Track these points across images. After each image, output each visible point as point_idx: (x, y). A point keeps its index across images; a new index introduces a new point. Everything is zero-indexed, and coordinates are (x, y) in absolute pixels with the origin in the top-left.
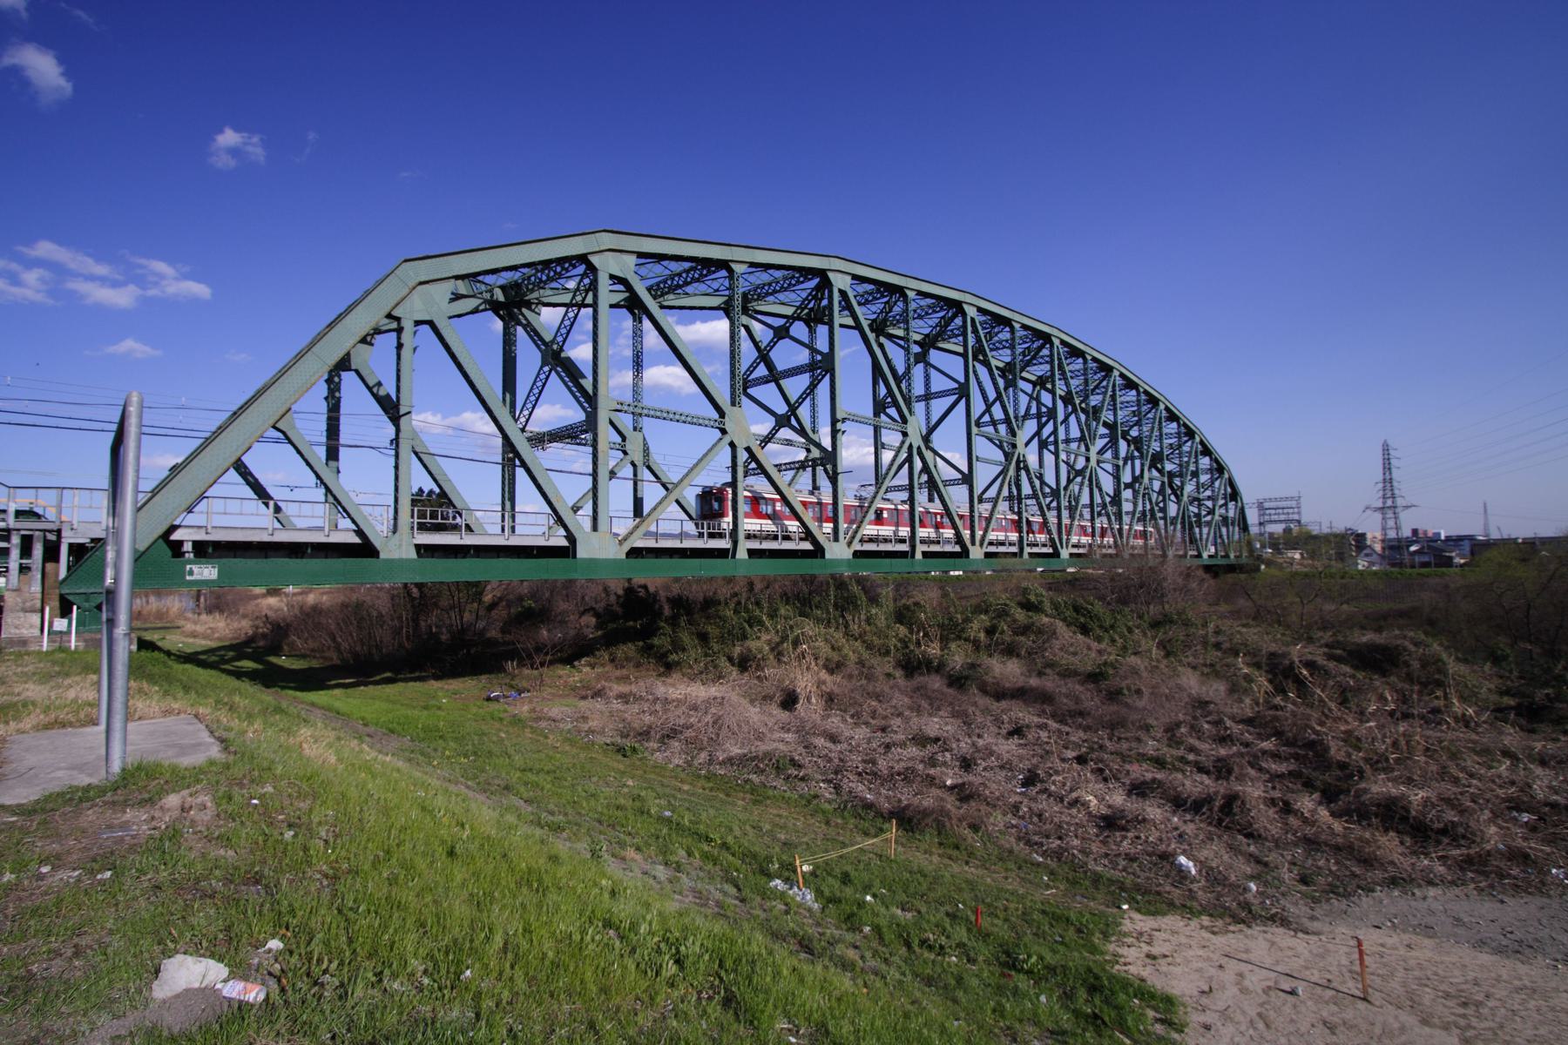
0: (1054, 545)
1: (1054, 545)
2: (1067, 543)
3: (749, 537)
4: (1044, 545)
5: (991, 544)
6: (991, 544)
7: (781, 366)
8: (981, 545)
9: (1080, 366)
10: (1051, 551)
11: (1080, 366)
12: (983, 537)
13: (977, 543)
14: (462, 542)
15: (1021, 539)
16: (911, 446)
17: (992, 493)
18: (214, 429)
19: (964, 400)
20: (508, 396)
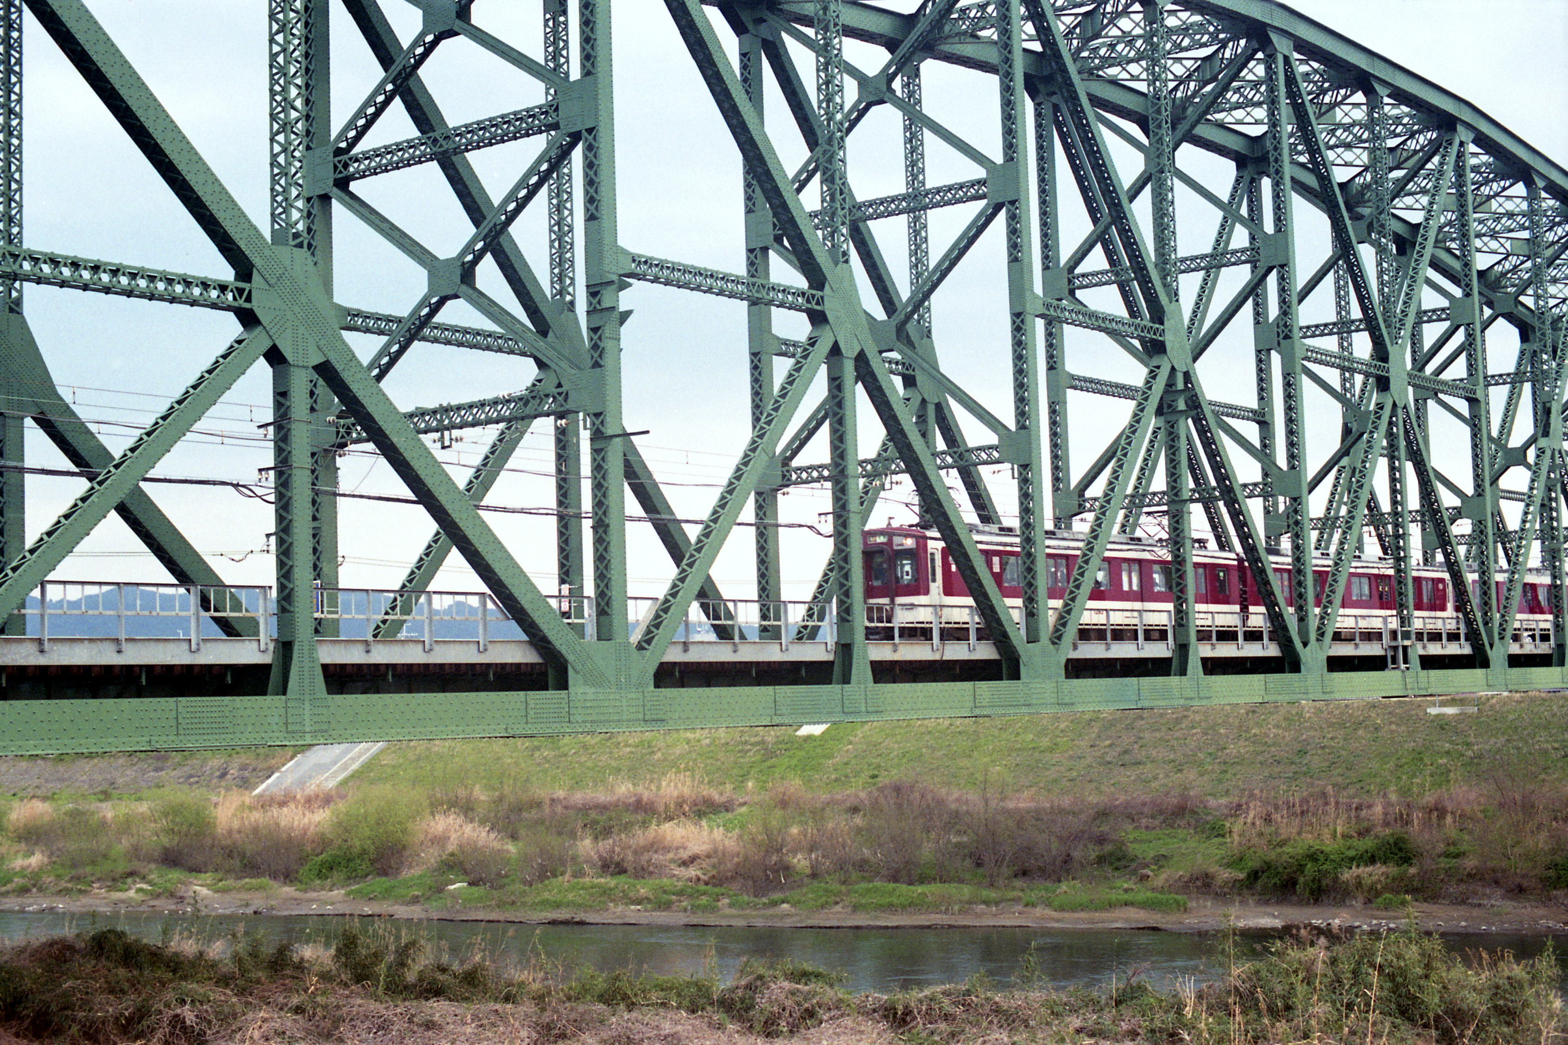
0: (1473, 636)
1: (1286, 643)
2: (1321, 634)
3: (1204, 635)
4: (1453, 637)
5: (1085, 634)
6: (1337, 637)
7: (898, 186)
8: (1057, 637)
9: (1359, 114)
10: (1467, 650)
11: (1359, 114)
12: (1062, 621)
13: (1313, 636)
14: (897, 657)
15: (1181, 617)
16: (835, 351)
17: (1097, 489)
18: (148, 421)
19: (1001, 218)
20: (1276, 359)
